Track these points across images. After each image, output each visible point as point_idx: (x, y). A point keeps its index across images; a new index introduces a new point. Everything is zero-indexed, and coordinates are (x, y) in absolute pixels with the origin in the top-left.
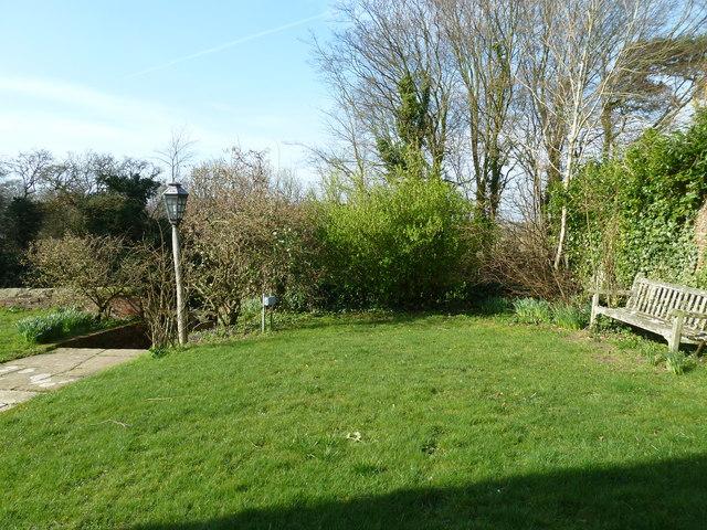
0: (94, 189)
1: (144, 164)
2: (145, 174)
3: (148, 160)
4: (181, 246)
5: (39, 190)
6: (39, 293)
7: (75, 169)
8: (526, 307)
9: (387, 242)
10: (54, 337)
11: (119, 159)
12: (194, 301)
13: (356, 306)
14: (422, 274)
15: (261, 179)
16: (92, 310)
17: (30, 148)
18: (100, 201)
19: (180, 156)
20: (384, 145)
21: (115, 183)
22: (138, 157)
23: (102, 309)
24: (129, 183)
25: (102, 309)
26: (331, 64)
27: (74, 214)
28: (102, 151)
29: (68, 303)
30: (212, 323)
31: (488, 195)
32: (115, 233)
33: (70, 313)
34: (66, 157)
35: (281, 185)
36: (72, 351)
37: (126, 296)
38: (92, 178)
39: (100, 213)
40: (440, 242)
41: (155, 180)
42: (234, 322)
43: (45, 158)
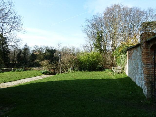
0: (45, 52)
1: (53, 47)
2: (53, 49)
3: (54, 47)
4: (61, 61)
5: (37, 53)
6: (41, 68)
7: (42, 49)
8: (107, 70)
9: (88, 61)
10: (44, 73)
11: (49, 47)
12: (62, 69)
13: (84, 70)
14: (92, 65)
15: (127, 8)
16: (48, 70)
17: (35, 45)
18: (46, 54)
19: (59, 46)
20: (94, 44)
21: (48, 51)
22: (52, 46)
23: (50, 70)
24: (51, 51)
25: (50, 70)
26: (85, 30)
27: (42, 56)
28: (46, 45)
29: (45, 69)
30: (64, 72)
31: (15, 53)
32: (49, 59)
33: (45, 71)
34: (40, 46)
35: (77, 50)
36: (47, 75)
37: (53, 69)
38: (45, 50)
39: (46, 56)
40: (96, 61)
41: (55, 50)
42: (67, 71)
43: (37, 46)
